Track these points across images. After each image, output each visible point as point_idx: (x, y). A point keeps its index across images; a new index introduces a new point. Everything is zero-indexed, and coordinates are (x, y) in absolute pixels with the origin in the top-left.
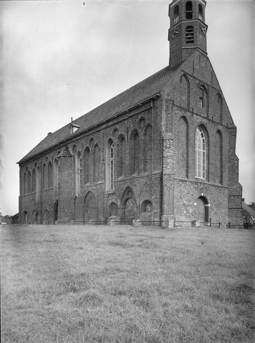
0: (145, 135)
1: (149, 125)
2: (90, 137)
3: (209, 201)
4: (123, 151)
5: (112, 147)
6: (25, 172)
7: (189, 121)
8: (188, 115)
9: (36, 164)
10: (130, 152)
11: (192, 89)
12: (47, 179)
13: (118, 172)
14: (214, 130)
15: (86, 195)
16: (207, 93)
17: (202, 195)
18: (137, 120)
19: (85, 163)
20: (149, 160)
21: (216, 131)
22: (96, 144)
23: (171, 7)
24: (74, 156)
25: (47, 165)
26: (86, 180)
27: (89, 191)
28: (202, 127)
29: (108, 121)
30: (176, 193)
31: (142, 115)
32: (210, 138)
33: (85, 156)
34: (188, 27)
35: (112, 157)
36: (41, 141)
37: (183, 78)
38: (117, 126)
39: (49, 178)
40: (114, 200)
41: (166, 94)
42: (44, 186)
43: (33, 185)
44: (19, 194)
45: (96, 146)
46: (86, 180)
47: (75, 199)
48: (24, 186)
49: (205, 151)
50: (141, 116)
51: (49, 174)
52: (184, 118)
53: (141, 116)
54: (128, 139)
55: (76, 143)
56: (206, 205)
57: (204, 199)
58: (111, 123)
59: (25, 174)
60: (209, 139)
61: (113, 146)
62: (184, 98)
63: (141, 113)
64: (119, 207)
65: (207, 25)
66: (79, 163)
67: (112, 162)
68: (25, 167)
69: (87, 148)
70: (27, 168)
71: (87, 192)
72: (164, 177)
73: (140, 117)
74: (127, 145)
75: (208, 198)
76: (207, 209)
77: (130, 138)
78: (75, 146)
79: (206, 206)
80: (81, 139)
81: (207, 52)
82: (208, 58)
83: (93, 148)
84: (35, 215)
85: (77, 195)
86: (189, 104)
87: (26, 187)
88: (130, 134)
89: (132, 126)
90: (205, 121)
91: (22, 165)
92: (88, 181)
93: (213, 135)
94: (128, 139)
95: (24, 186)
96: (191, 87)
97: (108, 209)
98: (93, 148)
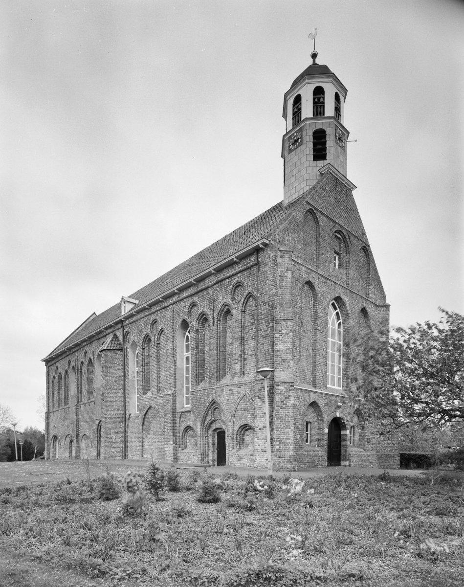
38: (196, 299)
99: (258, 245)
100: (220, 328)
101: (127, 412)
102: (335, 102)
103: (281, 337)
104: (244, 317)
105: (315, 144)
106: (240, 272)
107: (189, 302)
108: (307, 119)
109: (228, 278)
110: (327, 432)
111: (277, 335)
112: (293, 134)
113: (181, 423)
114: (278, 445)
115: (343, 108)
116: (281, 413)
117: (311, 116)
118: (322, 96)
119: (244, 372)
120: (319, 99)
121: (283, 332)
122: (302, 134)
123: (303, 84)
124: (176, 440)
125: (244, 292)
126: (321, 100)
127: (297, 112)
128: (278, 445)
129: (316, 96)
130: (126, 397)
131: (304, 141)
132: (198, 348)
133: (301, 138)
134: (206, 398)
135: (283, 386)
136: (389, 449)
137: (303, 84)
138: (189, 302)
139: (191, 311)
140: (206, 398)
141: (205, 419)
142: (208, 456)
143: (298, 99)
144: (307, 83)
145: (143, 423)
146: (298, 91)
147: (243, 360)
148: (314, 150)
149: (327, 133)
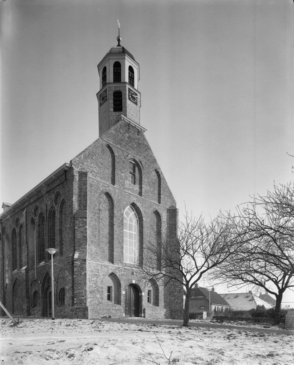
17: (134, 282)
38: (38, 204)
73: (55, 192)
99: (64, 168)
100: (50, 223)
101: (5, 283)
102: (129, 73)
103: (79, 229)
104: (61, 216)
105: (114, 101)
106: (58, 185)
107: (34, 206)
108: (109, 83)
109: (52, 189)
110: (143, 293)
111: (76, 228)
112: (102, 93)
113: (32, 289)
114: (76, 301)
115: (100, 85)
116: (77, 279)
117: (112, 81)
118: (119, 68)
119: (62, 252)
120: (117, 70)
121: (80, 225)
122: (106, 94)
123: (116, 57)
124: (29, 301)
125: (61, 199)
126: (119, 71)
127: (104, 78)
128: (76, 301)
129: (115, 68)
130: (4, 272)
131: (108, 98)
132: (40, 237)
133: (106, 96)
134: (43, 271)
135: (78, 261)
136: (178, 306)
137: (116, 57)
138: (34, 206)
139: (36, 211)
140: (43, 271)
141: (44, 286)
142: (47, 311)
143: (105, 69)
144: (109, 59)
145: (13, 290)
146: (104, 64)
147: (61, 244)
148: (114, 105)
149: (122, 93)
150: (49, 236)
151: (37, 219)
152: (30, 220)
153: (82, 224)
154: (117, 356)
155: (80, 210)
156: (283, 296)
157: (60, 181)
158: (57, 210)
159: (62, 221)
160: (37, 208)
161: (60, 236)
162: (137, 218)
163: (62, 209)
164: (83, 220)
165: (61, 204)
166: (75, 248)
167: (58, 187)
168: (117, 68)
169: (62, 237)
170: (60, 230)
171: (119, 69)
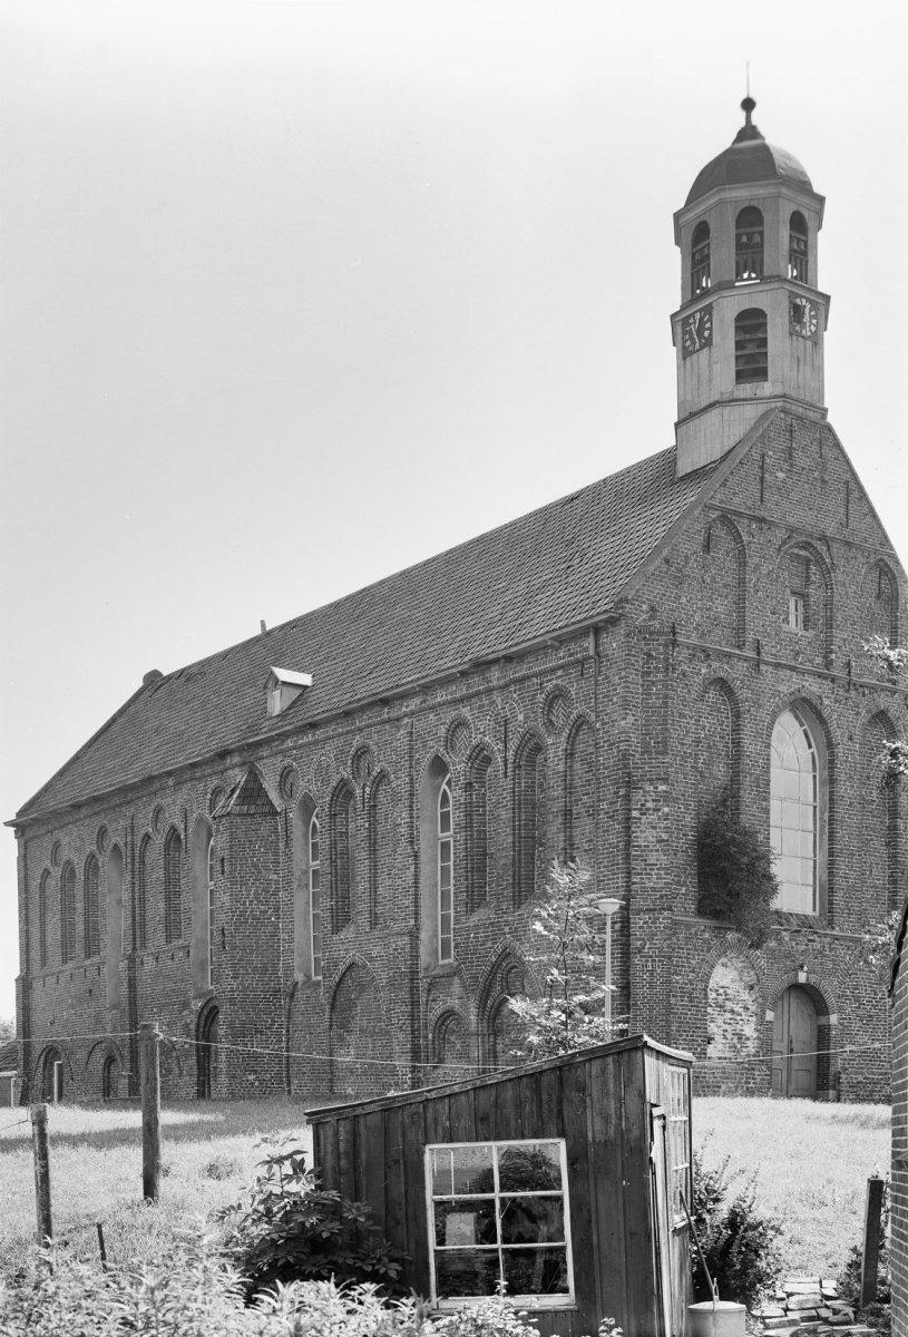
0: (570, 755)
1: (580, 723)
2: (357, 741)
3: (831, 1000)
4: (488, 808)
5: (444, 786)
6: (47, 863)
7: (743, 694)
8: (737, 672)
9: (102, 832)
10: (514, 817)
11: (757, 567)
12: (162, 905)
13: (470, 890)
14: (858, 714)
15: (337, 980)
16: (827, 572)
17: (802, 978)
18: (541, 698)
19: (333, 845)
20: (586, 851)
21: (864, 716)
22: (382, 771)
23: (682, 221)
24: (286, 813)
25: (159, 841)
26: (341, 918)
27: (352, 964)
28: (806, 708)
29: (427, 689)
30: (688, 976)
31: (557, 678)
32: (840, 751)
33: (333, 816)
34: (742, 316)
35: (445, 828)
36: (114, 711)
37: (720, 532)
38: (465, 712)
39: (168, 899)
40: (454, 1003)
41: (645, 607)
42: (144, 939)
43: (87, 929)
44: (18, 969)
45: (380, 782)
46: (341, 918)
47: (292, 995)
48: (43, 932)
49: (817, 804)
50: (554, 682)
51: (168, 881)
52: (723, 685)
53: (554, 682)
54: (506, 765)
55: (295, 760)
56: (823, 1020)
57: (811, 997)
58: (441, 696)
59: (47, 872)
60: (832, 754)
61: (449, 783)
62: (721, 607)
63: (553, 670)
64: (473, 1028)
65: (828, 293)
66: (307, 845)
67: (445, 846)
68: (48, 844)
69: (344, 783)
70: (57, 845)
71: (342, 968)
72: (634, 919)
73: (549, 686)
74: (504, 790)
75: (830, 989)
76: (822, 1036)
77: (514, 763)
78: (286, 774)
79: (820, 1023)
80: (316, 743)
81: (827, 404)
82: (830, 429)
83: (368, 790)
84: (102, 1061)
85: (299, 977)
86: (740, 630)
87: (54, 934)
88: (512, 745)
89: (521, 717)
90: (812, 686)
91: (29, 834)
92: (347, 920)
93: (851, 739)
94: (506, 765)
95: (43, 932)
96: (752, 562)
97: (430, 1036)
98: (368, 790)
132: (472, 827)
138: (449, 715)
150: (514, 826)
151: (458, 765)
152: (426, 763)
153: (653, 801)
154: (771, 1233)
155: (646, 756)
156: (706, 164)
157: (571, 655)
158: (552, 744)
159: (571, 784)
160: (460, 724)
161: (565, 832)
162: (810, 747)
163: (573, 745)
164: (656, 788)
165: (571, 730)
166: (629, 877)
167: (560, 673)
168: (748, 230)
169: (571, 836)
170: (565, 815)
171: (754, 233)
